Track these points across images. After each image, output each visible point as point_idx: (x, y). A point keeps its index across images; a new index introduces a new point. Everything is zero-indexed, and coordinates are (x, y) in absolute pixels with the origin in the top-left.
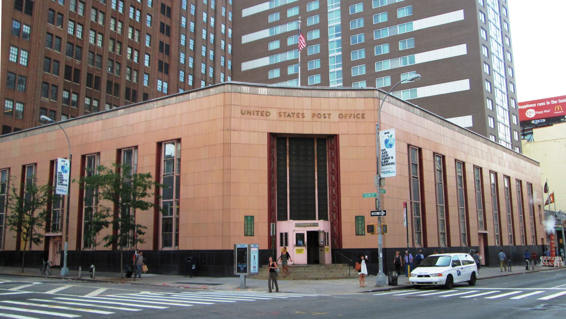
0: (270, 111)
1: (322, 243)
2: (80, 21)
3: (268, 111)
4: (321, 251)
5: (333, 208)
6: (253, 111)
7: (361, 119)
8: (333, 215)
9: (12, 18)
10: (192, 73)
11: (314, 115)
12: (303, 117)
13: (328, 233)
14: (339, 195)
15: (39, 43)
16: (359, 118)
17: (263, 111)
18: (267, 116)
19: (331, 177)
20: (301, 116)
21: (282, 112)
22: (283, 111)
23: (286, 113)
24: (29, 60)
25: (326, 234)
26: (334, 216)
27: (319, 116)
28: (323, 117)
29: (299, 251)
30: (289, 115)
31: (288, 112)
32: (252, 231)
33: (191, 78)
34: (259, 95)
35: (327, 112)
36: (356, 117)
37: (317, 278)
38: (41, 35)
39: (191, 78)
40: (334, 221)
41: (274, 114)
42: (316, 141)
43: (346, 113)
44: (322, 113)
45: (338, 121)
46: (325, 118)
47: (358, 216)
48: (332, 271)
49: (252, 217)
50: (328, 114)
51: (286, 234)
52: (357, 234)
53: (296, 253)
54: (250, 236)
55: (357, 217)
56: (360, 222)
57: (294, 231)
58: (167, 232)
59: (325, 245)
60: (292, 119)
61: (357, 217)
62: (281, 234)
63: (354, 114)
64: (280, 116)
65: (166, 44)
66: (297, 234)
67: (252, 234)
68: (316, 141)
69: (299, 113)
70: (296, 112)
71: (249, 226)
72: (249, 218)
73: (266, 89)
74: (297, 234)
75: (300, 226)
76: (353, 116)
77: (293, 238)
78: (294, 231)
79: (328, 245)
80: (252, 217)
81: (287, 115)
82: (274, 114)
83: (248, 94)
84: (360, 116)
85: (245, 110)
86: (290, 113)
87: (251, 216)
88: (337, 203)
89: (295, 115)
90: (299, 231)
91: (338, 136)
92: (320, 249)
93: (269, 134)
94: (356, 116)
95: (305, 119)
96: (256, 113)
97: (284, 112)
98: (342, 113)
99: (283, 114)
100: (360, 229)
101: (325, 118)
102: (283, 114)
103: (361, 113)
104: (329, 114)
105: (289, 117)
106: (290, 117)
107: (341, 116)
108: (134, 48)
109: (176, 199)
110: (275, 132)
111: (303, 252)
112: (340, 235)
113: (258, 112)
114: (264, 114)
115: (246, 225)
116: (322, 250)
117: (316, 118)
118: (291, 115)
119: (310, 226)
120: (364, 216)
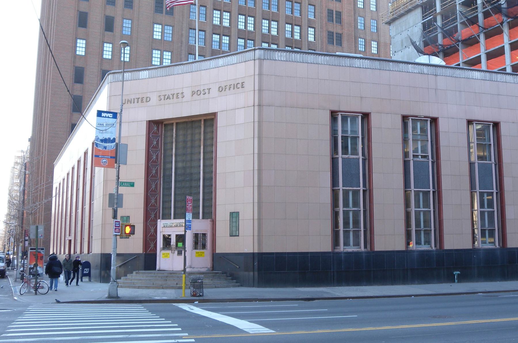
2: (226, 9)
3: (148, 96)
9: (153, 22)
10: (375, 37)
11: (193, 93)
15: (182, 41)
18: (147, 102)
22: (163, 93)
24: (172, 60)
30: (168, 98)
31: (167, 93)
33: (374, 44)
34: (141, 79)
35: (206, 87)
37: (139, 286)
38: (183, 32)
39: (374, 44)
41: (154, 99)
47: (233, 212)
48: (166, 280)
49: (238, 213)
52: (231, 236)
55: (232, 214)
56: (234, 220)
60: (171, 101)
61: (232, 214)
65: (336, 11)
70: (176, 92)
72: (125, 218)
73: (147, 72)
80: (238, 213)
81: (166, 97)
82: (154, 99)
83: (130, 80)
84: (239, 86)
85: (125, 99)
87: (127, 216)
89: (175, 96)
94: (236, 86)
95: (184, 99)
97: (164, 94)
100: (234, 229)
107: (221, 89)
108: (294, 23)
109: (343, 187)
113: (173, 95)
114: (144, 100)
115: (231, 221)
117: (195, 96)
120: (121, 216)
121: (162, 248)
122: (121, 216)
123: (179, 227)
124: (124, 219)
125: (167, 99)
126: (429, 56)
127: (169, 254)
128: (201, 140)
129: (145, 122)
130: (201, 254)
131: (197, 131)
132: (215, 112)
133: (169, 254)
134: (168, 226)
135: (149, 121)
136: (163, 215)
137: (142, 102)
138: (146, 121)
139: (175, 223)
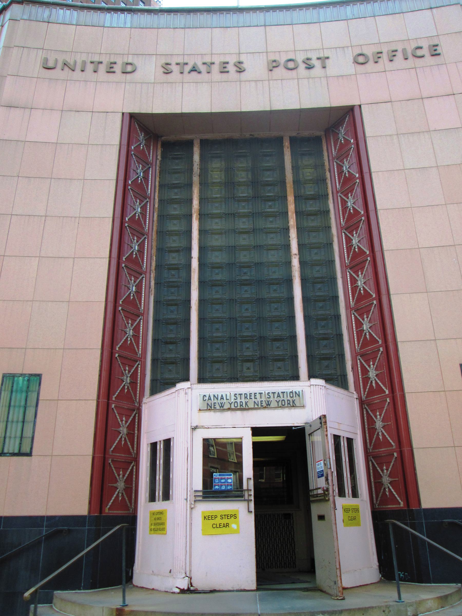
0: (135, 62)
1: (321, 482)
4: (321, 522)
5: (365, 344)
6: (84, 63)
7: (429, 60)
8: (365, 371)
12: (240, 71)
13: (350, 441)
14: (365, 169)
16: (423, 57)
17: (112, 60)
19: (347, 237)
20: (231, 68)
21: (174, 63)
23: (187, 64)
25: (344, 445)
26: (372, 374)
27: (291, 65)
28: (302, 66)
29: (218, 521)
30: (194, 69)
32: (28, 433)
36: (410, 56)
40: (372, 392)
42: (287, 144)
43: (379, 50)
44: (300, 58)
45: (352, 71)
46: (310, 67)
50: (318, 59)
51: (168, 443)
53: (205, 532)
54: (14, 454)
57: (194, 428)
58: (207, 489)
59: (342, 493)
62: (154, 446)
63: (404, 51)
64: (168, 72)
66: (207, 443)
67: (26, 449)
68: (287, 144)
69: (227, 63)
71: (16, 414)
74: (207, 443)
75: (222, 406)
76: (399, 55)
77: (189, 457)
78: (194, 428)
79: (355, 494)
81: (187, 68)
84: (425, 51)
86: (199, 64)
88: (385, 370)
90: (216, 427)
91: (357, 111)
92: (316, 510)
93: (127, 119)
96: (90, 67)
98: (365, 52)
99: (175, 69)
101: (310, 67)
102: (175, 69)
103: (425, 44)
104: (323, 60)
105: (194, 74)
106: (200, 73)
110: (149, 111)
111: (234, 526)
112: (406, 449)
114: (118, 68)
116: (321, 518)
117: (280, 72)
118: (203, 69)
119: (268, 406)
121: (201, 494)
122: (5, 372)
123: (275, 408)
124: (18, 383)
125: (189, 73)
126: (30, 391)
127: (235, 516)
128: (287, 181)
129: (118, 118)
130: (225, 521)
131: (269, 163)
132: (355, 105)
133: (235, 516)
134: (225, 407)
135: (133, 116)
136: (153, 381)
137: (110, 71)
138: (121, 114)
139: (258, 396)
